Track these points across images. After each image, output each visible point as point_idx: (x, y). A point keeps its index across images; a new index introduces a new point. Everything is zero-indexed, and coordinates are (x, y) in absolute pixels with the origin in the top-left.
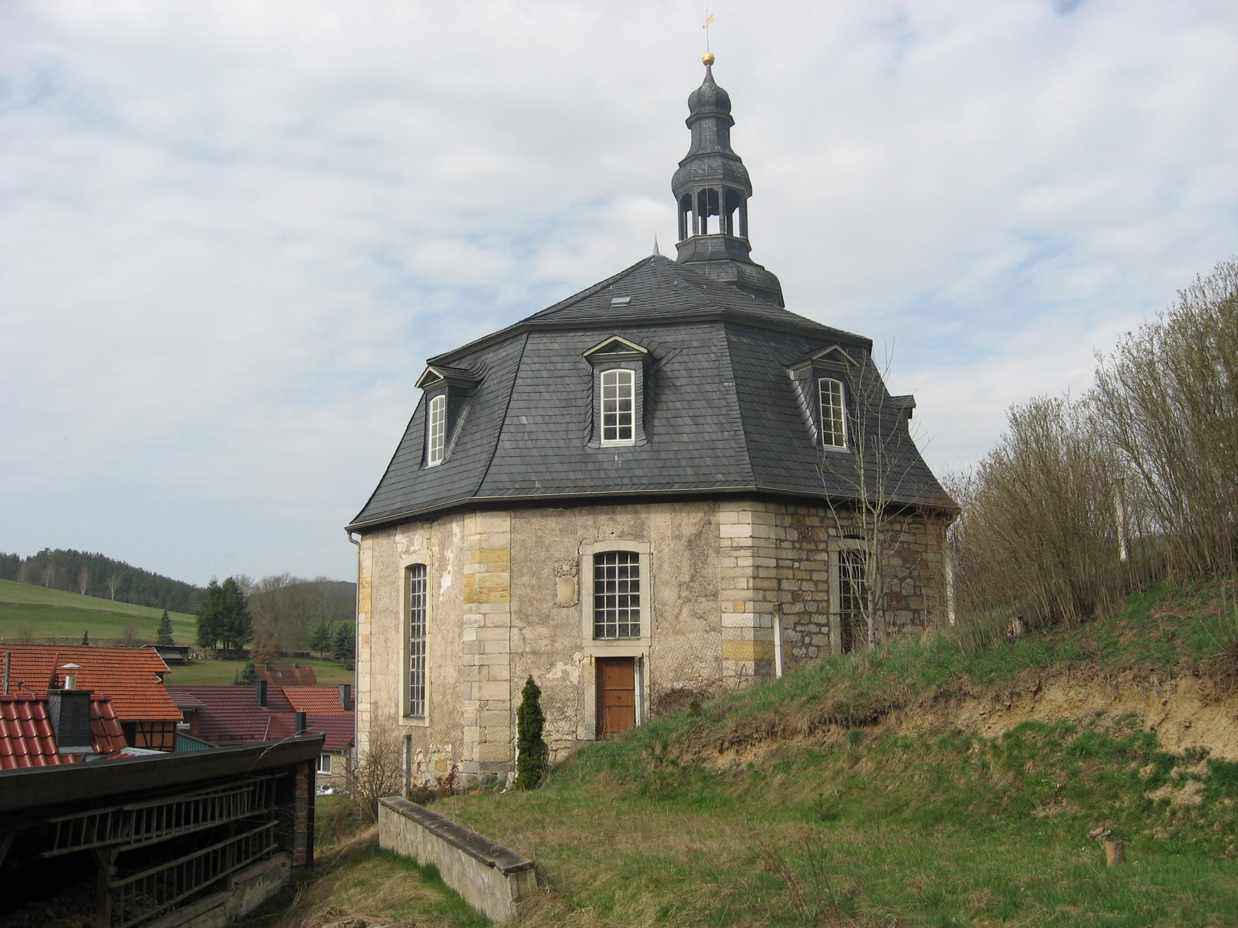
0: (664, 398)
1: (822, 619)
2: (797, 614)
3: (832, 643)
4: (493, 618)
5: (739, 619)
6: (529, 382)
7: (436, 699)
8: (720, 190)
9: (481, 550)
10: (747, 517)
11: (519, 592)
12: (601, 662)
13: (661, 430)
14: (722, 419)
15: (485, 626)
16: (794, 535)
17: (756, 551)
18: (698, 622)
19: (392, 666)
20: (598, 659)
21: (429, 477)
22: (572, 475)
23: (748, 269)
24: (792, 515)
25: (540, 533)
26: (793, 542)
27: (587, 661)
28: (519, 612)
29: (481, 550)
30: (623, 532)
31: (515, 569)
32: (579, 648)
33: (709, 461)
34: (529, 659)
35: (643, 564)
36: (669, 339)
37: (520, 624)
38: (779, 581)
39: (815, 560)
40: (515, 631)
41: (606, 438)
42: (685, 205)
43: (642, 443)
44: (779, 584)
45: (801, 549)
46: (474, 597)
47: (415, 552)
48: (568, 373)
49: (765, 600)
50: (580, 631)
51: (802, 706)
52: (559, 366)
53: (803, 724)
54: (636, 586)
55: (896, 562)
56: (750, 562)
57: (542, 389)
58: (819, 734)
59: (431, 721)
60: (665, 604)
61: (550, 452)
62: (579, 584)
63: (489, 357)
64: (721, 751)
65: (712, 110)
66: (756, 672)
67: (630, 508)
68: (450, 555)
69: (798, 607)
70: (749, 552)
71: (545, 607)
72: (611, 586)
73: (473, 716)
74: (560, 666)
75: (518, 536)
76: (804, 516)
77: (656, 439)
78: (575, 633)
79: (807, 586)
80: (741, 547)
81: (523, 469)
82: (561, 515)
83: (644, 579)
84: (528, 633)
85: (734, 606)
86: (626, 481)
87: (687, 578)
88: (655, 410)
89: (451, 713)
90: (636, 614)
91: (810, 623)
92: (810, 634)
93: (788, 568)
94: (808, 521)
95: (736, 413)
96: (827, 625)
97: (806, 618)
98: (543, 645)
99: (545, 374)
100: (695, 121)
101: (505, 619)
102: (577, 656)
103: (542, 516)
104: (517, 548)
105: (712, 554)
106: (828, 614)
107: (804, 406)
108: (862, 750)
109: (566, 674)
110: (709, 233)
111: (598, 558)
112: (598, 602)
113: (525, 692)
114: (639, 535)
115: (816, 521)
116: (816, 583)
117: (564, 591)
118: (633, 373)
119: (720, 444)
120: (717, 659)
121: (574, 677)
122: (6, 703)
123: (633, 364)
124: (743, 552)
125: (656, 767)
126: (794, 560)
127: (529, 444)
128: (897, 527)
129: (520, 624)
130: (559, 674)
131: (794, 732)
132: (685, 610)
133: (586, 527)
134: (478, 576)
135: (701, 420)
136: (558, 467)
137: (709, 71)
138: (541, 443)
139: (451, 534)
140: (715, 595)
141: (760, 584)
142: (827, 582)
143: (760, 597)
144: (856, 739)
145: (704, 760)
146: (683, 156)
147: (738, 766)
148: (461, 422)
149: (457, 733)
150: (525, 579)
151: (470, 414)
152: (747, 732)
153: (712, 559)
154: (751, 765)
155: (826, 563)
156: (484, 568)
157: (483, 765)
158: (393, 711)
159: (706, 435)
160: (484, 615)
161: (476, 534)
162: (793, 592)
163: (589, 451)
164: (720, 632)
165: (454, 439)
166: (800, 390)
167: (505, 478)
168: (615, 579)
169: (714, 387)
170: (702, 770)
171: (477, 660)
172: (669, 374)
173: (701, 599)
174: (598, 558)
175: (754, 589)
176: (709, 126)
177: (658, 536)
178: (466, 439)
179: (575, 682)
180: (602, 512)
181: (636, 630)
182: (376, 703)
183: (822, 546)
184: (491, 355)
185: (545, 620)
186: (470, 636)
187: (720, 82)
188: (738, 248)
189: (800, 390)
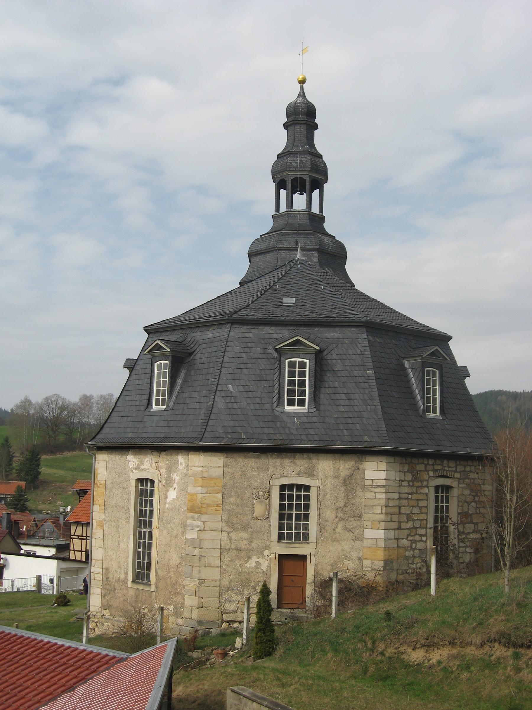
0: (326, 379)
1: (423, 532)
2: (409, 529)
3: (428, 547)
4: (210, 525)
5: (376, 534)
6: (233, 360)
7: (160, 573)
8: (307, 179)
9: (203, 478)
10: (383, 466)
11: (228, 508)
12: (282, 558)
13: (326, 402)
14: (366, 397)
15: (204, 530)
16: (409, 477)
17: (387, 488)
18: (348, 534)
19: (122, 545)
20: (280, 555)
21: (155, 418)
22: (266, 430)
23: (326, 239)
24: (409, 464)
25: (244, 469)
26: (409, 481)
27: (273, 556)
28: (228, 522)
29: (203, 478)
30: (300, 471)
31: (226, 492)
32: (268, 547)
33: (358, 427)
34: (234, 553)
35: (313, 494)
36: (329, 336)
37: (228, 530)
38: (400, 507)
39: (421, 493)
40: (225, 534)
42: (280, 185)
43: (312, 410)
44: (400, 510)
45: (412, 486)
46: (196, 509)
48: (261, 356)
49: (391, 521)
50: (269, 536)
51: (474, 628)
52: (253, 350)
53: (477, 639)
54: (307, 507)
55: (467, 492)
56: (383, 496)
57: (242, 366)
58: (487, 648)
59: (156, 587)
60: (327, 521)
61: (250, 413)
62: (269, 505)
63: (198, 335)
64: (414, 649)
65: (302, 118)
66: (385, 568)
67: (305, 455)
68: (175, 477)
69: (410, 525)
70: (383, 490)
71: (246, 519)
72: (290, 507)
73: (194, 589)
74: (254, 559)
75: (229, 470)
77: (322, 408)
78: (265, 537)
79: (416, 510)
80: (379, 486)
81: (232, 423)
82: (259, 457)
83: (313, 503)
84: (233, 536)
85: (372, 524)
86: (304, 437)
87: (342, 505)
88: (320, 387)
89: (173, 585)
91: (416, 534)
92: (415, 542)
93: (405, 499)
95: (375, 393)
96: (425, 535)
97: (414, 531)
98: (244, 544)
99: (244, 356)
100: (290, 125)
101: (218, 525)
102: (266, 552)
103: (246, 458)
104: (228, 478)
106: (426, 528)
107: (415, 386)
108: (521, 663)
109: (258, 564)
110: (293, 208)
111: (283, 488)
112: (281, 517)
113: (262, 592)
114: (311, 474)
116: (421, 508)
117: (259, 509)
118: (308, 362)
119: (365, 415)
120: (359, 559)
121: (264, 566)
123: (308, 356)
124: (379, 489)
125: (370, 655)
126: (408, 494)
127: (235, 406)
128: (468, 469)
129: (228, 530)
130: (254, 564)
131: (470, 644)
132: (340, 526)
133: (275, 467)
134: (200, 496)
135: (352, 396)
136: (256, 424)
137: (302, 88)
138: (244, 406)
139: (177, 463)
140: (360, 516)
142: (426, 507)
143: (389, 519)
144: (517, 656)
145: (402, 653)
146: (280, 151)
147: (429, 660)
148: (180, 381)
149: (179, 599)
150: (232, 500)
151: (186, 376)
152: (436, 640)
153: (359, 493)
154: (439, 662)
155: (427, 495)
156: (204, 490)
157: (200, 623)
158: (122, 576)
159: (355, 407)
160: (204, 522)
161: (199, 466)
162: (407, 515)
163: (277, 414)
164: (362, 541)
165: (175, 393)
166: (411, 375)
167: (220, 429)
168: (294, 502)
169: (360, 374)
170: (402, 661)
171: (197, 552)
172: (329, 362)
174: (283, 488)
175: (386, 514)
176: (301, 129)
177: (324, 475)
178: (185, 395)
179: (265, 570)
180: (287, 457)
181: (306, 537)
182: (107, 569)
183: (425, 483)
184: (199, 334)
185: (245, 528)
186: (192, 535)
187: (310, 98)
188: (317, 221)
189: (411, 375)
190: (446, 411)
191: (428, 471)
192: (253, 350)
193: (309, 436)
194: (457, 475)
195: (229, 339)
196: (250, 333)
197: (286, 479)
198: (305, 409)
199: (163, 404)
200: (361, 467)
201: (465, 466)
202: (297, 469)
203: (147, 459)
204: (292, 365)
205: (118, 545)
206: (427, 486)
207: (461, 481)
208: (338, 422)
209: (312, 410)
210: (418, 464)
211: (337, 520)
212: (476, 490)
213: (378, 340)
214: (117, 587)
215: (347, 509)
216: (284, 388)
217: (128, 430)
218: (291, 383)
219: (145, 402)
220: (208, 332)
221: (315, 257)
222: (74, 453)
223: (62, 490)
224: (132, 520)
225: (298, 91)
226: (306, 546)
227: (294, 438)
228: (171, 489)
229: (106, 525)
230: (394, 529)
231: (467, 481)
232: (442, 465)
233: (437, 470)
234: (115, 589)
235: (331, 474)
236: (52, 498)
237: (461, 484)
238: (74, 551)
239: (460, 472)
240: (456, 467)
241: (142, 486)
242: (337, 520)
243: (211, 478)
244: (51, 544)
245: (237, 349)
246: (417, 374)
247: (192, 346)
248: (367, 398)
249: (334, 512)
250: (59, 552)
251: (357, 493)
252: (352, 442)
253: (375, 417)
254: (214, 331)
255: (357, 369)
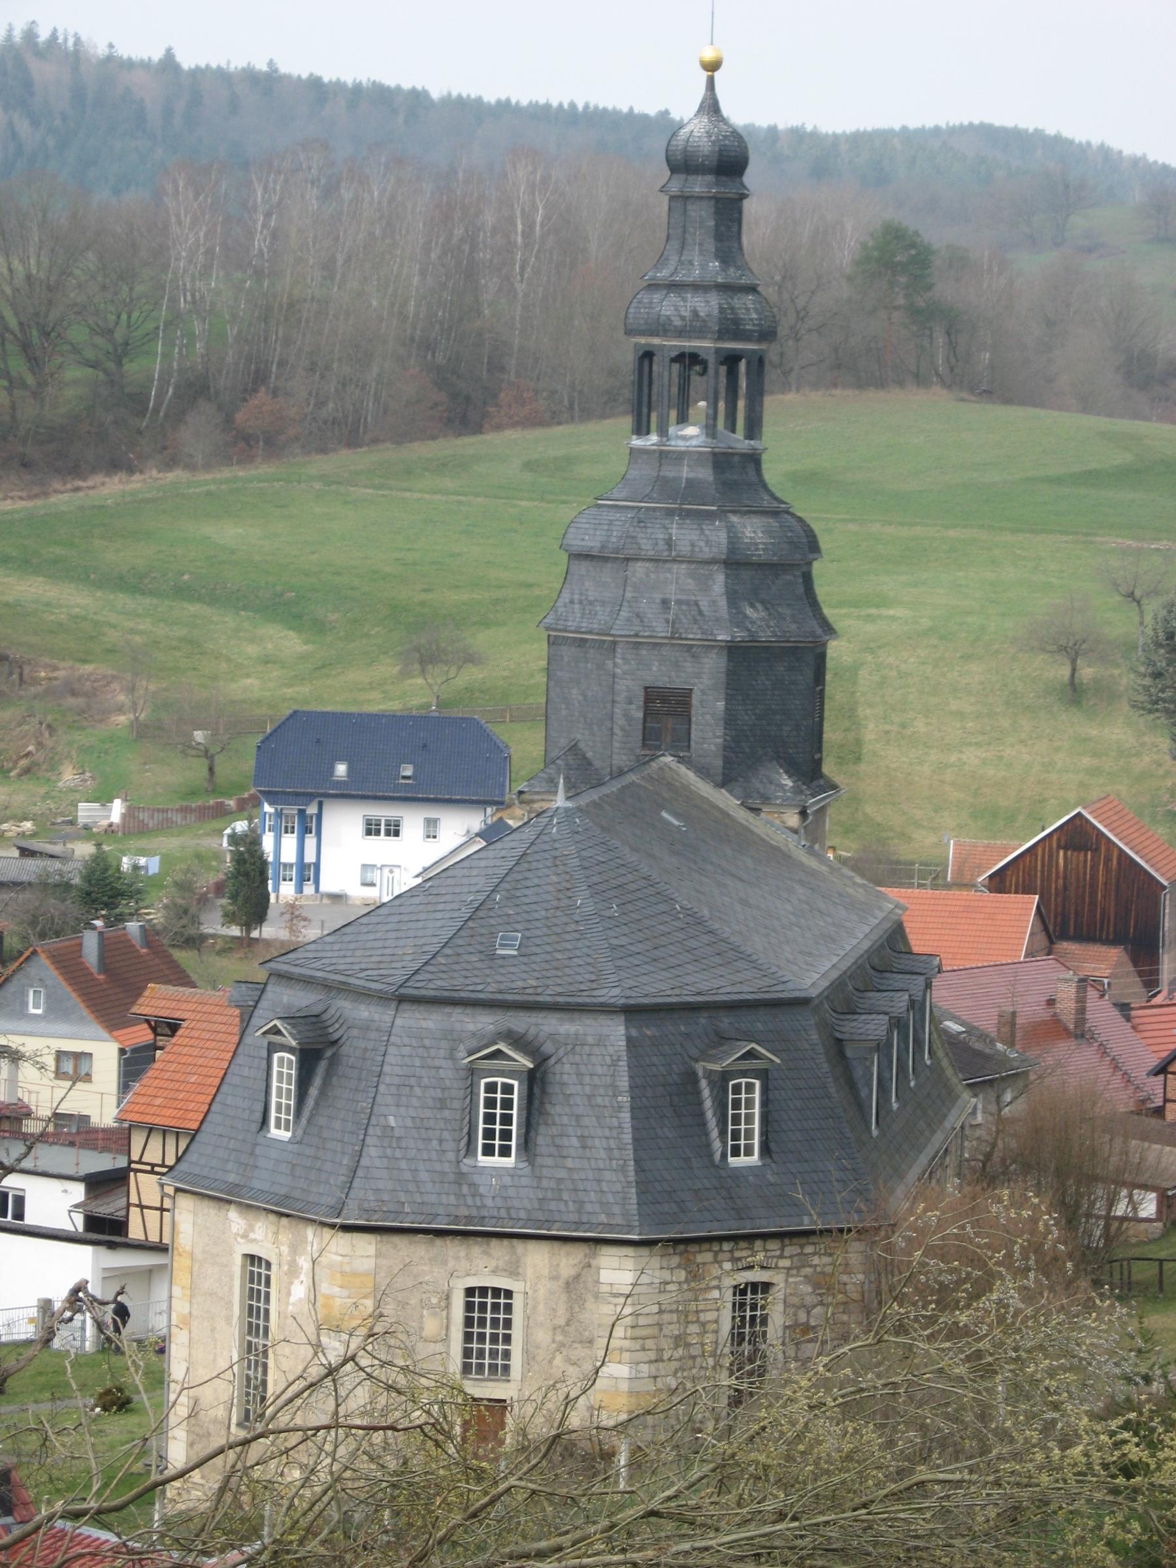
6: (398, 1070)
9: (343, 1273)
10: (629, 1264)
24: (681, 1254)
26: (680, 1283)
29: (343, 1273)
30: (497, 1267)
35: (517, 1302)
41: (485, 1154)
47: (254, 1241)
48: (443, 1063)
54: (508, 1324)
57: (413, 1081)
62: (448, 1318)
76: (695, 1253)
83: (517, 1317)
86: (503, 1213)
87: (562, 1322)
90: (507, 1354)
94: (700, 1258)
95: (628, 1137)
104: (383, 1274)
105: (590, 1298)
114: (514, 1271)
115: (708, 1257)
122: (142, 1566)
127: (398, 1153)
133: (457, 1258)
134: (338, 1301)
135: (589, 1142)
137: (711, 84)
139: (304, 1240)
141: (639, 1332)
142: (716, 1322)
148: (313, 1092)
153: (590, 1304)
156: (345, 1293)
161: (336, 1254)
163: (464, 1169)
168: (487, 1310)
173: (576, 1345)
174: (470, 1292)
177: (534, 1277)
190: (772, 1146)
191: (720, 1263)
192: (433, 1052)
193: (512, 1211)
194: (785, 1263)
195: (394, 1031)
196: (431, 1021)
197: (475, 1278)
198: (510, 1161)
199: (287, 1129)
200: (594, 1263)
201: (802, 1246)
202: (493, 1264)
203: (259, 1224)
204: (491, 1088)
205: (214, 1360)
206: (718, 1287)
207: (794, 1272)
208: (562, 1187)
209: (522, 1165)
210: (700, 1252)
211: (554, 1345)
212: (823, 1284)
213: (649, 1033)
214: (211, 1431)
215: (571, 1329)
216: (477, 1126)
217: (230, 1166)
218: (490, 1118)
219: (258, 1116)
220: (363, 1007)
221: (719, 581)
222: (136, 483)
223: (80, 701)
224: (235, 1320)
225: (698, 92)
226: (505, 1385)
227: (486, 1214)
228: (297, 1282)
229: (195, 1323)
230: (651, 1362)
231: (808, 1270)
232: (752, 1249)
233: (739, 1259)
234: (209, 1434)
235: (546, 1272)
236: (40, 745)
237: (792, 1276)
238: (142, 1207)
239: (791, 1257)
240: (782, 1249)
241: (252, 1264)
242: (554, 1345)
243: (355, 1274)
244: (71, 1171)
245: (406, 1051)
246: (715, 1091)
247: (337, 1026)
248: (614, 1146)
249: (550, 1333)
250: (96, 1197)
251: (587, 1304)
252: (578, 1225)
253: (623, 1179)
254: (372, 1009)
255: (602, 1091)
